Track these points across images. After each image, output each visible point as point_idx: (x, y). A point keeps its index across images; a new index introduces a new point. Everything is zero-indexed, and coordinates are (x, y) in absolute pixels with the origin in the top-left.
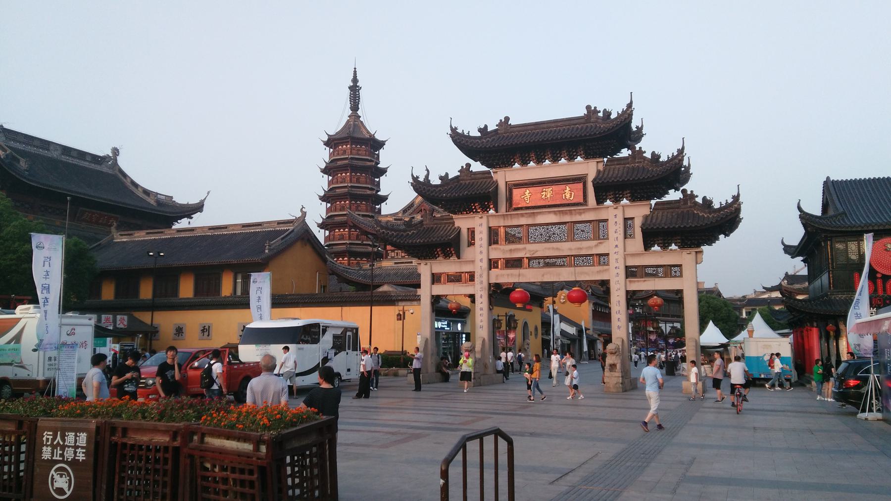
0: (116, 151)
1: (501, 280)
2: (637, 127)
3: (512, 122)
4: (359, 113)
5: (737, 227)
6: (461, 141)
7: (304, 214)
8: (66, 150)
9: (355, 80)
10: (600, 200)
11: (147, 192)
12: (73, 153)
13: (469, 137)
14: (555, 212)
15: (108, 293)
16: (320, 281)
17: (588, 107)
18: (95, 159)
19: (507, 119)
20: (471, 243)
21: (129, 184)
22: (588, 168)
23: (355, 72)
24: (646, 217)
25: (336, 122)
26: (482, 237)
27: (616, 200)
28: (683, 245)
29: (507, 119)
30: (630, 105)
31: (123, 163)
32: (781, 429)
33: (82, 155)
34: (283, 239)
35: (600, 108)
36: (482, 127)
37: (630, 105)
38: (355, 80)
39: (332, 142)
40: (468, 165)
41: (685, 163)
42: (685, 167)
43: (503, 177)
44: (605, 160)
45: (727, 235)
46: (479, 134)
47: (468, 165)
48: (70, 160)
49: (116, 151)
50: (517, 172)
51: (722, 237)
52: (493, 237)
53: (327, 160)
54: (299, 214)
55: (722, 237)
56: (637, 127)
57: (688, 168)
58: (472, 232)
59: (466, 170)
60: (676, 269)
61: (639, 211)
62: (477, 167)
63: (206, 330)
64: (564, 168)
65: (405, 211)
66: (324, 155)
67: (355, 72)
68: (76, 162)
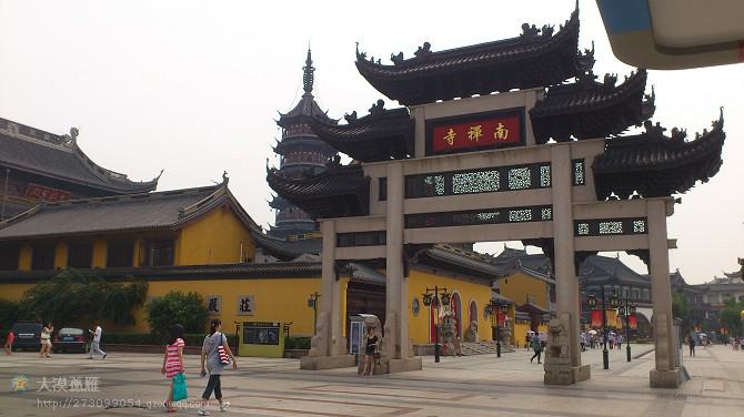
0: (75, 132)
1: (416, 241)
2: (587, 51)
3: (434, 49)
4: (313, 93)
5: (718, 170)
6: (367, 68)
7: (226, 180)
8: (24, 129)
9: (309, 61)
10: (541, 140)
11: (101, 171)
12: (46, 137)
13: (379, 66)
14: (484, 155)
15: (25, 264)
16: (244, 253)
17: (525, 26)
18: (54, 138)
19: (427, 45)
20: (383, 197)
21: (86, 163)
22: (520, 98)
23: (309, 53)
24: (598, 159)
25: (290, 101)
26: (395, 188)
27: (562, 138)
28: (649, 193)
29: (427, 45)
30: (575, 15)
31: (82, 143)
32: (721, 379)
33: (40, 134)
34: (199, 206)
35: (539, 26)
36: (396, 54)
37: (575, 15)
38: (309, 61)
39: (285, 121)
40: (381, 103)
41: (648, 91)
42: (647, 97)
43: (423, 114)
44: (547, 89)
45: (705, 180)
46: (392, 64)
47: (381, 103)
48: (29, 139)
49: (75, 132)
50: (440, 109)
51: (698, 182)
52: (415, 187)
53: (280, 139)
54: (221, 181)
55: (698, 182)
56: (587, 51)
57: (651, 99)
58: (383, 181)
59: (378, 108)
60: (639, 223)
61: (592, 149)
62: (391, 105)
63: (245, 306)
64: (495, 101)
65: (726, 342)
66: (278, 134)
67: (309, 53)
68: (34, 140)
